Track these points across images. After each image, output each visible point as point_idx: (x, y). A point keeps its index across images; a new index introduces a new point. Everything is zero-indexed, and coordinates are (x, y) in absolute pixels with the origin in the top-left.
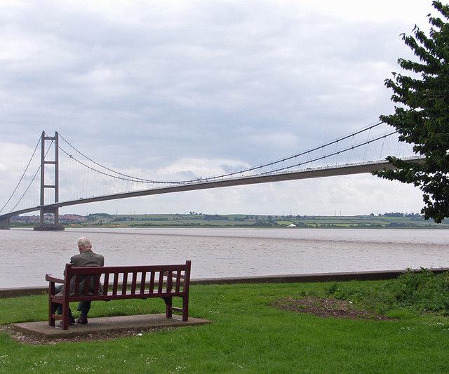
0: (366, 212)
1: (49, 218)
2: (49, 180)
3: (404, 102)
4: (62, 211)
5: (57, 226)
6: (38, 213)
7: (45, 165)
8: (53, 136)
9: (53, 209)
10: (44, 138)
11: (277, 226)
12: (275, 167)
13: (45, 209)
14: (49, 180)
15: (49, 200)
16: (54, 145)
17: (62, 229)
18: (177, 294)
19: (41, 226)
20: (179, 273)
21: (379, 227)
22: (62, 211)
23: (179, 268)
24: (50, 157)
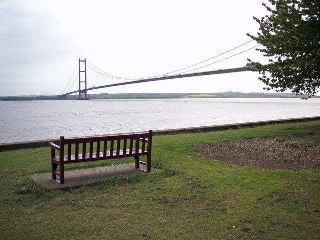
0: (218, 92)
1: (83, 95)
2: (83, 79)
3: (280, 52)
4: (88, 92)
5: (87, 98)
6: (78, 93)
7: (65, 165)
8: (84, 60)
9: (84, 91)
10: (80, 61)
11: (181, 97)
12: (185, 70)
13: (80, 91)
14: (83, 79)
15: (83, 88)
16: (84, 64)
17: (89, 100)
18: (143, 153)
19: (79, 98)
20: (144, 139)
21: (223, 97)
22: (88, 92)
23: (144, 136)
24: (83, 74)
